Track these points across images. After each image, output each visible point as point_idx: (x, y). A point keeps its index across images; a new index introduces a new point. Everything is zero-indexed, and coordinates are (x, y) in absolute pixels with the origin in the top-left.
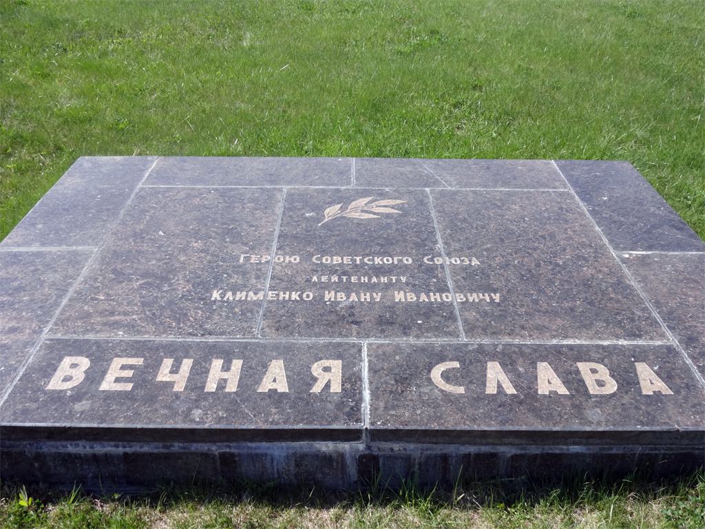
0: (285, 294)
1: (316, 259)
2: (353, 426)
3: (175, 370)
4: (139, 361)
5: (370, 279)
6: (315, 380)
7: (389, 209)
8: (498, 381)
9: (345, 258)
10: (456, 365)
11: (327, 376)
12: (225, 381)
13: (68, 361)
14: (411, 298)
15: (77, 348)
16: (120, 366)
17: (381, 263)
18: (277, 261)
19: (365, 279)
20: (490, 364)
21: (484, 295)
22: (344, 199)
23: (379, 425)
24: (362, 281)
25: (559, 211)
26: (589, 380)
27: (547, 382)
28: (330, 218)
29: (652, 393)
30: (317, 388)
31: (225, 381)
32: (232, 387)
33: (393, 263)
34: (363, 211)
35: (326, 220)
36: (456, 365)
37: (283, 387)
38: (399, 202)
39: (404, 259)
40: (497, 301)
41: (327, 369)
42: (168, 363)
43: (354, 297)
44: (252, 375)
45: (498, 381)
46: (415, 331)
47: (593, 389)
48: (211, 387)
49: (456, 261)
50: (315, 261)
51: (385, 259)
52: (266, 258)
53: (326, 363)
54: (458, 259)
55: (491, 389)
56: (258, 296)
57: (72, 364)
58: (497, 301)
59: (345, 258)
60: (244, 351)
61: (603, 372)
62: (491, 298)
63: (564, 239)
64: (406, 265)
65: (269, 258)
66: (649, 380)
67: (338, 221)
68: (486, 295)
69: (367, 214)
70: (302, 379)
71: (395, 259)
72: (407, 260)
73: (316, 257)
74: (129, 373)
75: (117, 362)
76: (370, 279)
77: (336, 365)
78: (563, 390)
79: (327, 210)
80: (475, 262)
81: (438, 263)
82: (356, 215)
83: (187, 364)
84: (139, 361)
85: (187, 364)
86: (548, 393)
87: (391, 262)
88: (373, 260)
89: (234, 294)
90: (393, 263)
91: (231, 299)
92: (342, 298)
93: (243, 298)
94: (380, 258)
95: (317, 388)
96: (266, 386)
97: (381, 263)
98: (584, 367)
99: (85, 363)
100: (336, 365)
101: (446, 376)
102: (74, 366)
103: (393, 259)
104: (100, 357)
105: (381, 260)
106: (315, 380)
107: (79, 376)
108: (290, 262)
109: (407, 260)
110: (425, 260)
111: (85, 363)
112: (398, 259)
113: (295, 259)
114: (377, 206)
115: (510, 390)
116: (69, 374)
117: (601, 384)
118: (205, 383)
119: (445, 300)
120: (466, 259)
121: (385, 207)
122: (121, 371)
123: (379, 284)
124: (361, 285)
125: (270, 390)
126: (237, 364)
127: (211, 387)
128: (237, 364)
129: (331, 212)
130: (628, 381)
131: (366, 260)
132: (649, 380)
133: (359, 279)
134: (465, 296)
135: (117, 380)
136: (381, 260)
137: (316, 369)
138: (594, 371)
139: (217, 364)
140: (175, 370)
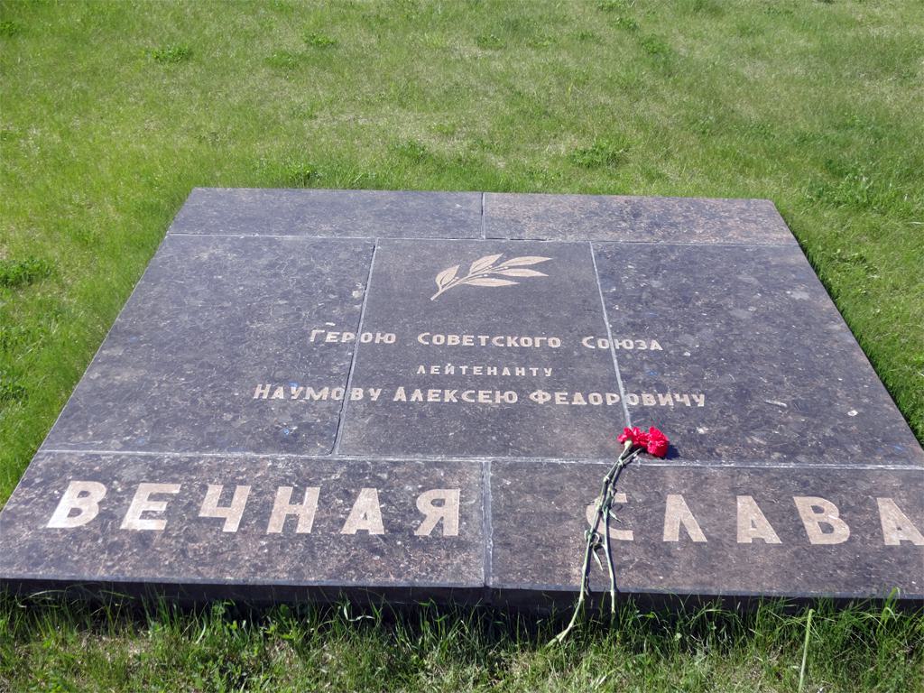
1: (498, 341)
3: (226, 500)
4: (175, 489)
5: (500, 370)
6: (423, 518)
7: (527, 270)
9: (465, 337)
11: (441, 511)
13: (76, 486)
14: (649, 402)
17: (516, 345)
19: (450, 369)
21: (681, 397)
22: (464, 258)
24: (517, 374)
25: (516, 109)
28: (446, 288)
32: (304, 527)
35: (441, 291)
37: (375, 527)
39: (551, 340)
40: (701, 404)
42: (215, 491)
44: (331, 517)
45: (682, 524)
47: (816, 537)
48: (275, 526)
49: (627, 344)
50: (497, 344)
51: (523, 340)
53: (435, 494)
54: (631, 343)
55: (670, 534)
56: (320, 394)
58: (701, 404)
59: (465, 337)
61: (832, 514)
63: (91, 45)
64: (600, 350)
65: (352, 336)
68: (686, 396)
69: (497, 280)
70: (400, 520)
71: (538, 340)
72: (554, 342)
73: (498, 338)
75: (144, 490)
76: (500, 370)
80: (655, 345)
83: (242, 495)
84: (175, 489)
85: (242, 495)
86: (899, 543)
87: (442, 341)
88: (505, 341)
91: (372, 390)
92: (453, 341)
93: (265, 397)
94: (516, 338)
95: (425, 530)
96: (350, 529)
97: (516, 345)
98: (803, 504)
99: (98, 491)
102: (84, 494)
105: (516, 341)
106: (423, 518)
107: (90, 512)
108: (381, 341)
109: (554, 342)
110: (420, 339)
111: (98, 491)
113: (389, 339)
114: (510, 268)
115: (697, 535)
116: (435, 509)
117: (827, 528)
119: (599, 395)
120: (644, 342)
121: (523, 268)
122: (71, 519)
125: (358, 531)
127: (275, 526)
128: (312, 495)
129: (446, 278)
131: (494, 341)
132: (895, 526)
133: (484, 371)
134: (657, 399)
136: (516, 341)
137: (423, 503)
138: (817, 510)
139: (284, 493)
140: (226, 500)
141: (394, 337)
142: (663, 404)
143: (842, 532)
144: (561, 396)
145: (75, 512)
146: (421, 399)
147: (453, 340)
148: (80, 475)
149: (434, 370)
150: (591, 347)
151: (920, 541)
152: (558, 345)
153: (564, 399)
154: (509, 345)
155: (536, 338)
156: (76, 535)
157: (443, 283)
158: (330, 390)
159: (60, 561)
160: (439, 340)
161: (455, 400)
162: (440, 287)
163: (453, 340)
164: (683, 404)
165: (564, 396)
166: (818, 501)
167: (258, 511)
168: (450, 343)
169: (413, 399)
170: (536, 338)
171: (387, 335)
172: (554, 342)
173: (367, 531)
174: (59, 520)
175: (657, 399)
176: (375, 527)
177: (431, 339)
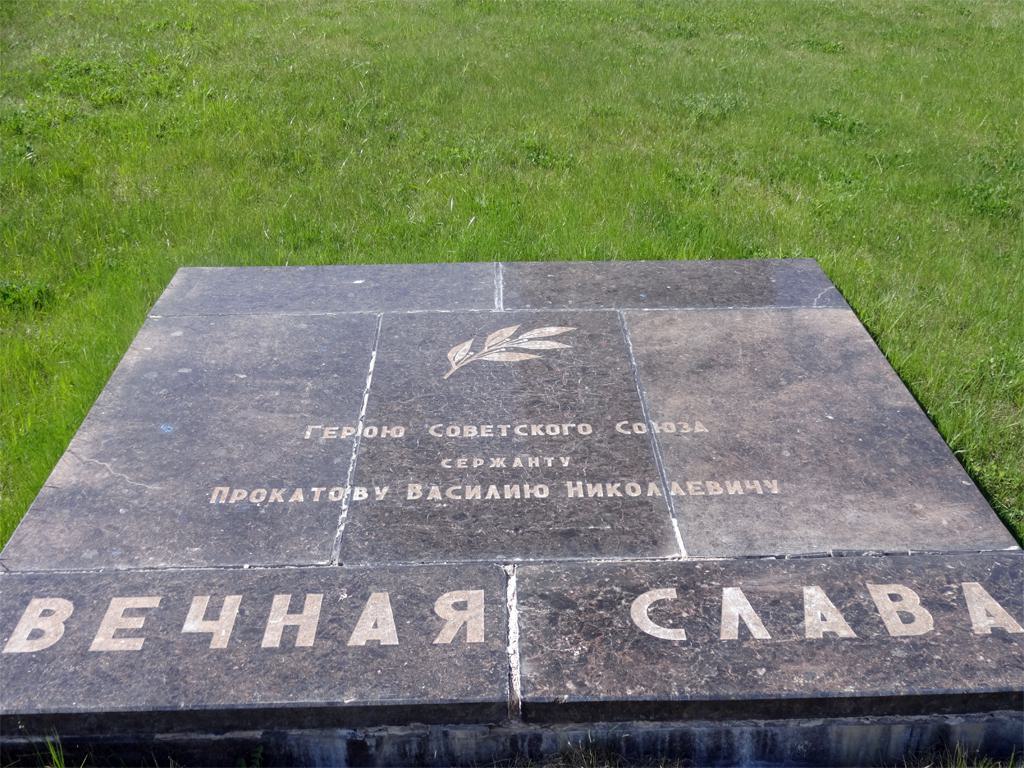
0: (574, 485)
1: (436, 431)
2: (490, 694)
3: (212, 614)
4: (152, 602)
8: (740, 618)
9: (483, 428)
10: (670, 594)
11: (466, 615)
12: (296, 628)
13: (37, 605)
15: (54, 584)
16: (469, 606)
18: (366, 434)
19: (498, 462)
20: (728, 592)
22: (477, 331)
23: (546, 692)
26: (888, 611)
27: (372, 624)
28: (460, 365)
29: (990, 632)
30: (446, 636)
31: (296, 628)
32: (306, 639)
33: (561, 433)
34: (508, 350)
36: (670, 594)
37: (388, 635)
38: (564, 329)
39: (580, 427)
41: (461, 606)
42: (199, 605)
43: (493, 490)
44: (334, 624)
45: (740, 618)
46: (22, 563)
47: (895, 628)
48: (271, 639)
52: (349, 431)
53: (458, 596)
55: (729, 632)
57: (461, 609)
59: (483, 428)
60: (325, 581)
61: (911, 600)
62: (685, 489)
64: (637, 436)
66: (984, 612)
67: (473, 369)
68: (579, 483)
71: (565, 427)
74: (138, 623)
75: (118, 605)
77: (476, 597)
78: (845, 631)
79: (490, 337)
81: (638, 432)
82: (495, 357)
83: (232, 604)
84: (152, 602)
86: (822, 636)
89: (500, 487)
90: (561, 433)
93: (479, 497)
95: (446, 636)
96: (359, 638)
98: (879, 594)
99: (64, 608)
100: (476, 597)
101: (659, 613)
102: (46, 613)
103: (561, 427)
104: (88, 600)
107: (53, 631)
109: (585, 429)
111: (64, 608)
112: (569, 428)
114: (530, 340)
117: (908, 618)
118: (295, 638)
121: (542, 339)
123: (470, 469)
124: (461, 473)
126: (314, 604)
127: (271, 639)
128: (314, 604)
129: (459, 354)
130: (781, 610)
134: (722, 485)
135: (121, 633)
137: (444, 606)
139: (281, 601)
140: (212, 614)
141: (402, 430)
142: (731, 492)
143: (924, 623)
144: (694, 485)
145: (36, 634)
146: (497, 497)
147: (471, 432)
148: (218, 484)
149: (461, 463)
150: (623, 431)
151: (1012, 626)
152: (401, 434)
153: (699, 488)
154: (534, 433)
155: (563, 425)
156: (42, 657)
157: (456, 360)
158: (231, 492)
159: (93, 692)
160: (453, 431)
161: (619, 494)
162: (453, 364)
163: (471, 432)
164: (753, 493)
165: (698, 485)
166: (894, 588)
167: (249, 628)
168: (457, 429)
169: (489, 497)
170: (563, 425)
171: (394, 429)
172: (585, 429)
173: (379, 641)
174: (19, 643)
175: (725, 489)
176: (388, 635)
177: (631, 428)
